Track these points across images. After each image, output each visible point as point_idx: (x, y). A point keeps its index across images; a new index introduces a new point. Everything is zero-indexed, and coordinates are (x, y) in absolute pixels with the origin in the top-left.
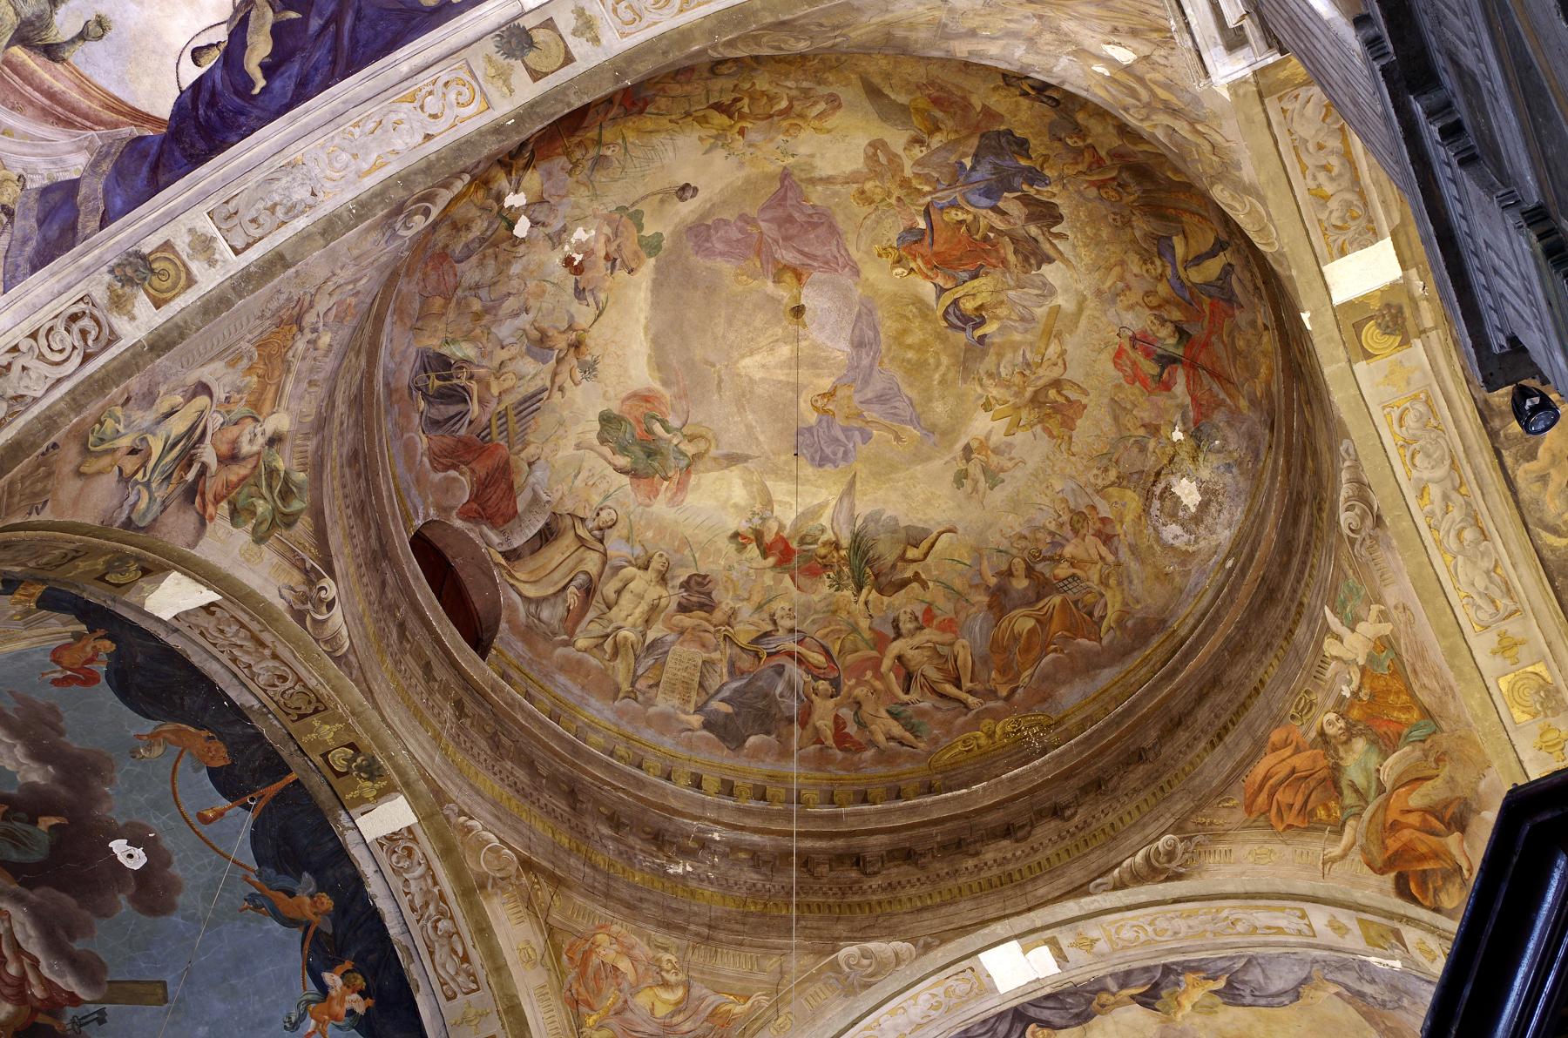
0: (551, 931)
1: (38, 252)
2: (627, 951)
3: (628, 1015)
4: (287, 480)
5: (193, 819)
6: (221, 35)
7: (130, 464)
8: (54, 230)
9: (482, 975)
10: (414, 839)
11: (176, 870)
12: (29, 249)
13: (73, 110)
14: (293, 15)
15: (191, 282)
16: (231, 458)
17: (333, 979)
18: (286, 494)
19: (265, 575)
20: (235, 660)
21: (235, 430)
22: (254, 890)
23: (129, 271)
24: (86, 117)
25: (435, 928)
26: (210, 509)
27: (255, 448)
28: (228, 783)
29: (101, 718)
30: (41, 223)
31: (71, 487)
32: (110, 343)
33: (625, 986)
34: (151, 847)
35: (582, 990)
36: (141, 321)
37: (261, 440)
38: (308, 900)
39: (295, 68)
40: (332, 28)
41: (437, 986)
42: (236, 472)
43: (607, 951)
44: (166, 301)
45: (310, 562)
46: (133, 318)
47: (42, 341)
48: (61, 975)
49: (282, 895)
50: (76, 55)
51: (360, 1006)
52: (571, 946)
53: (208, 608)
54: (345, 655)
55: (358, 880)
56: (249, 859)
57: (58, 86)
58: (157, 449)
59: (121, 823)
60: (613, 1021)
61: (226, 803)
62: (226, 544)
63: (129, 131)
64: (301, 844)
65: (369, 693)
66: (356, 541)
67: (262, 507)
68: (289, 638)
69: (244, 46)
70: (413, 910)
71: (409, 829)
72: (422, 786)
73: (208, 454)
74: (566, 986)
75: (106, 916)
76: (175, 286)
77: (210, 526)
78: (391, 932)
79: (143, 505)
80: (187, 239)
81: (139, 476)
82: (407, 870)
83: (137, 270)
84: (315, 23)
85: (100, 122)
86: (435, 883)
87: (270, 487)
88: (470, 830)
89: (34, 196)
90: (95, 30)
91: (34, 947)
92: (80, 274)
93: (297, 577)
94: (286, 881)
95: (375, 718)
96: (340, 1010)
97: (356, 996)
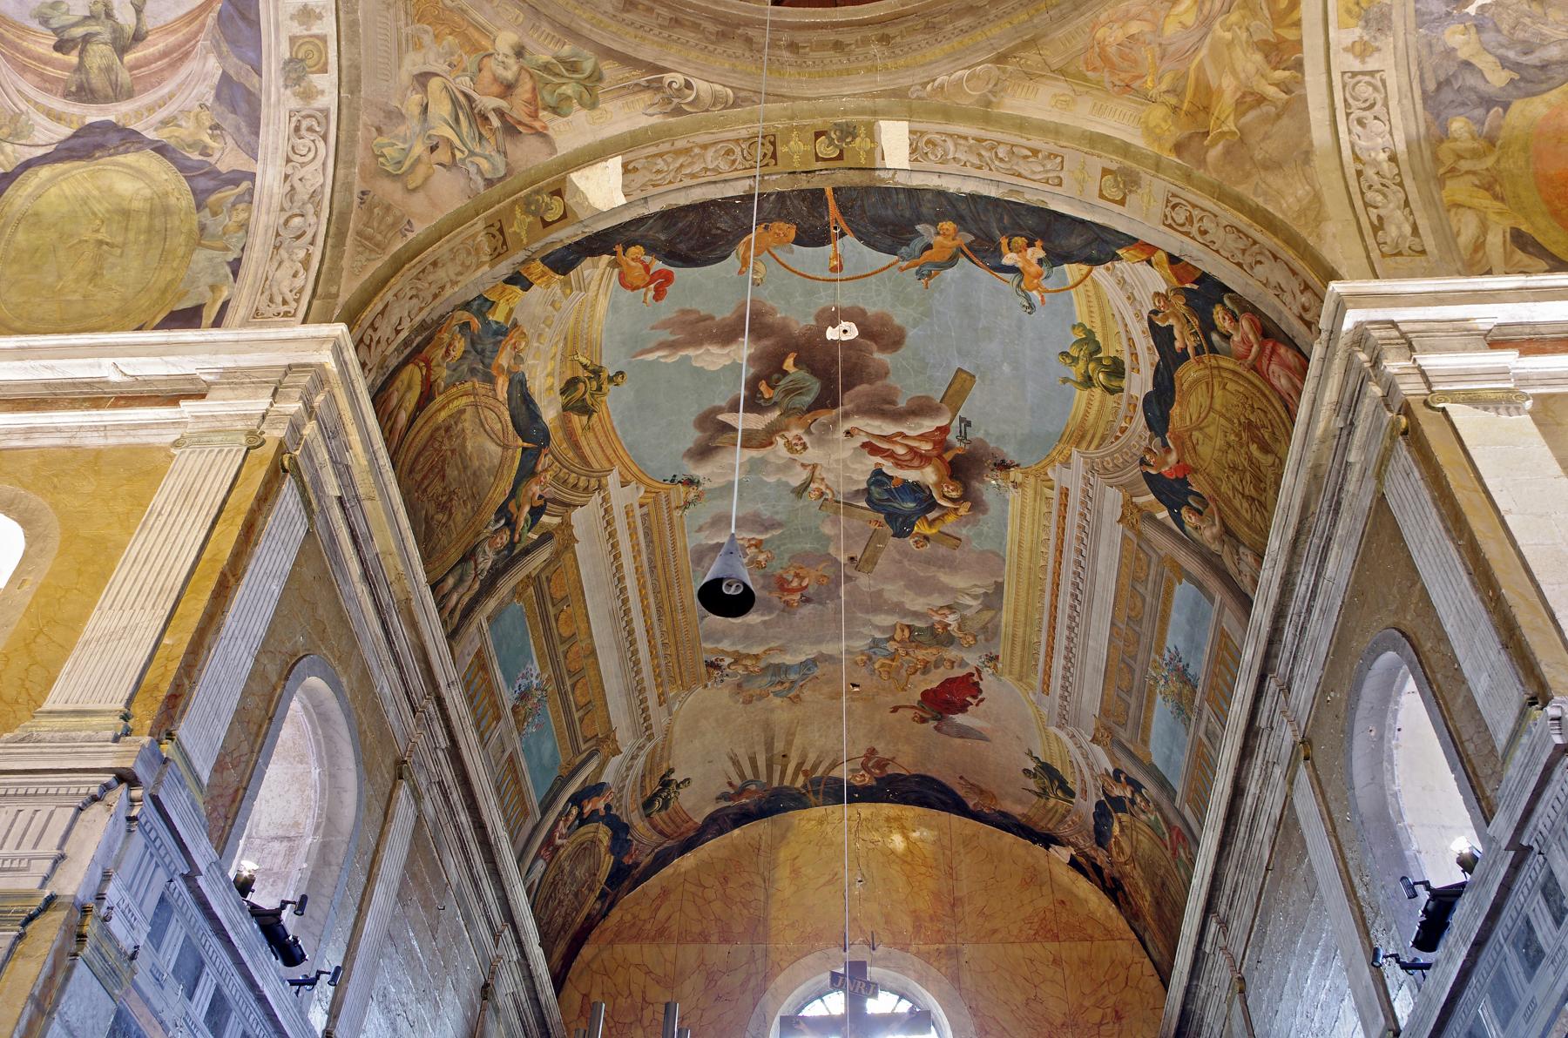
0: (1062, 72)
2: (1127, 18)
3: (1171, 49)
4: (562, 61)
5: (828, 275)
7: (443, 155)
8: (243, 107)
9: (1052, 147)
10: (922, 133)
11: (871, 310)
12: (245, 130)
13: (180, 46)
15: (323, 39)
16: (508, 89)
17: (1009, 259)
18: (573, 67)
19: (625, 116)
20: (693, 176)
21: (486, 74)
22: (915, 269)
23: (294, 75)
24: (188, 41)
25: (1001, 160)
26: (537, 125)
27: (515, 68)
28: (813, 236)
29: (705, 287)
30: (234, 112)
31: (418, 203)
32: (327, 117)
33: (1149, 37)
34: (848, 315)
35: (1123, 75)
36: (326, 85)
37: (512, 61)
38: (939, 238)
41: (1047, 188)
42: (524, 90)
43: (1112, 36)
44: (326, 64)
45: (643, 81)
46: (322, 92)
47: (295, 158)
48: (921, 426)
49: (927, 253)
50: (149, 24)
51: (1036, 253)
52: (1086, 63)
53: (626, 169)
54: (736, 97)
55: (940, 194)
56: (888, 259)
57: (161, 46)
58: (449, 133)
59: (813, 323)
60: (1165, 65)
61: (829, 248)
62: (573, 131)
63: (211, 19)
64: (890, 218)
65: (781, 97)
66: (692, 42)
67: (568, 90)
68: (697, 128)
70: (980, 168)
71: (911, 132)
72: (881, 102)
73: (489, 102)
74: (1109, 86)
75: (887, 373)
76: (320, 52)
77: (550, 132)
78: (993, 195)
79: (485, 165)
80: (296, 24)
81: (459, 155)
82: (946, 153)
83: (297, 70)
86: (966, 138)
87: (556, 75)
88: (942, 87)
89: (216, 105)
91: (889, 428)
92: (278, 104)
93: (646, 97)
94: (917, 244)
95: (805, 105)
96: (1035, 268)
97: (1030, 250)
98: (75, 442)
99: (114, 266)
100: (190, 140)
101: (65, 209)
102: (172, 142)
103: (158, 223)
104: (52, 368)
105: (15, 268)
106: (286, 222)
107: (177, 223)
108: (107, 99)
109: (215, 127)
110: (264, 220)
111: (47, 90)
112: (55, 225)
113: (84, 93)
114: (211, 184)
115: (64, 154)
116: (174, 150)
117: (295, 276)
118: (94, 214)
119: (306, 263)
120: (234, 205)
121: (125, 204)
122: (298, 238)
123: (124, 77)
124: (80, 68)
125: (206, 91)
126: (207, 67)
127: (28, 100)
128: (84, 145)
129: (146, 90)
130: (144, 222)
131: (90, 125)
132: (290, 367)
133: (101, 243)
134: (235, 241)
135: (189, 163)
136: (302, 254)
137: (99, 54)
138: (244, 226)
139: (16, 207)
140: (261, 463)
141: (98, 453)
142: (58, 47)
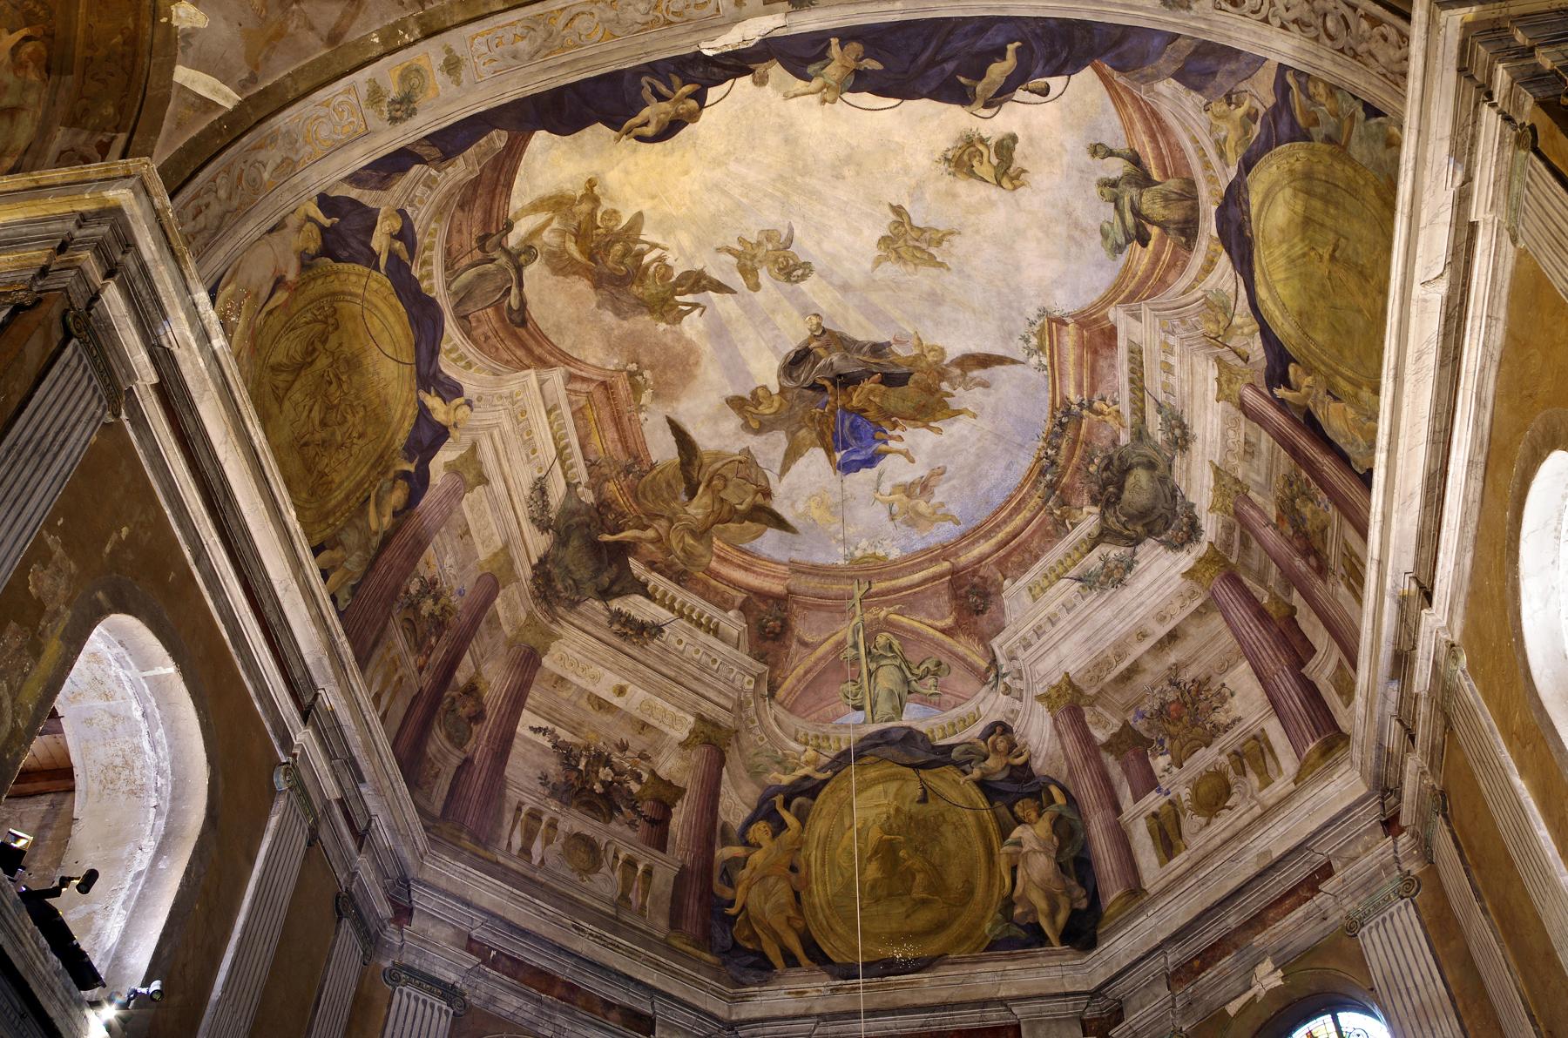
1: (1229, 60)
6: (1020, 94)
8: (1209, 62)
12: (1233, 66)
13: (1146, 119)
14: (962, 80)
30: (1214, 74)
39: (981, 44)
40: (939, 58)
50: (1121, 145)
57: (1145, 139)
69: (1008, 78)
84: (950, 66)
85: (1134, 98)
90: (1099, 150)
98: (1497, 357)
99: (1355, 249)
100: (1240, 131)
101: (1297, 283)
102: (1241, 151)
103: (1320, 190)
104: (1420, 355)
105: (1347, 353)
106: (1331, 37)
107: (1321, 167)
108: (1195, 209)
109: (1228, 97)
110: (1328, 65)
111: (1184, 266)
112: (1311, 299)
113: (1188, 230)
114: (1285, 118)
115: (1246, 268)
116: (1249, 151)
117: (1385, 39)
118: (1304, 255)
119: (1375, 22)
120: (1309, 97)
121: (1298, 219)
122: (1347, 26)
123: (1173, 184)
124: (1163, 226)
125: (1192, 101)
126: (1169, 96)
127: (1192, 287)
128: (1239, 246)
129: (1188, 166)
130: (1317, 204)
131: (1219, 233)
132: (1461, 70)
133: (1333, 258)
134: (1347, 105)
135: (1263, 137)
136: (1365, 25)
137: (1151, 204)
138: (1332, 90)
139: (1292, 332)
140: (1553, 137)
141: (1511, 335)
142: (1144, 244)
